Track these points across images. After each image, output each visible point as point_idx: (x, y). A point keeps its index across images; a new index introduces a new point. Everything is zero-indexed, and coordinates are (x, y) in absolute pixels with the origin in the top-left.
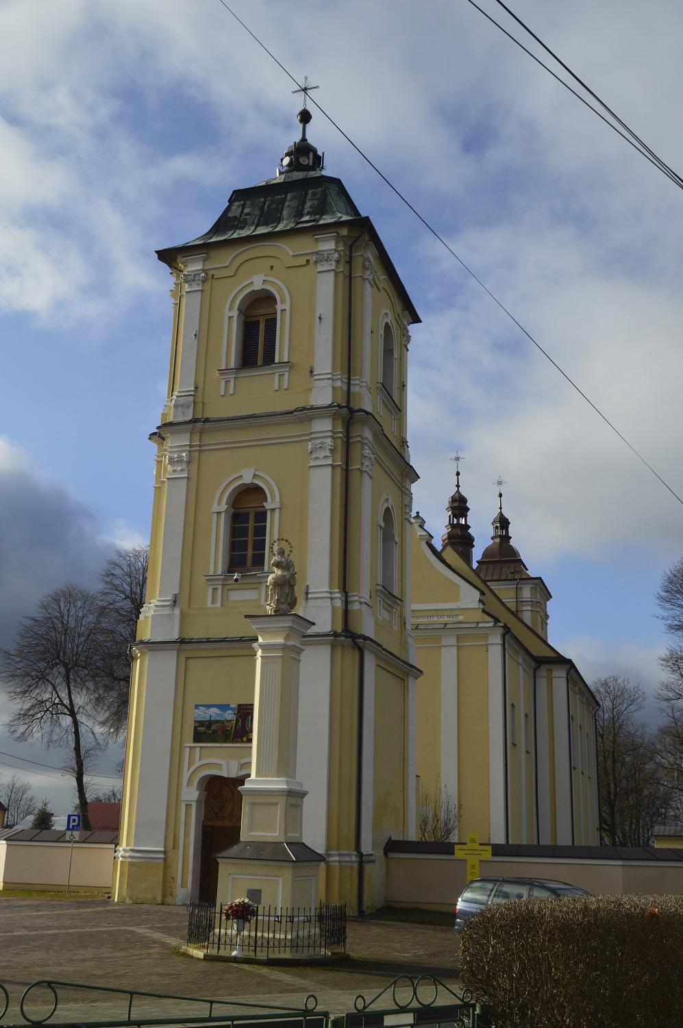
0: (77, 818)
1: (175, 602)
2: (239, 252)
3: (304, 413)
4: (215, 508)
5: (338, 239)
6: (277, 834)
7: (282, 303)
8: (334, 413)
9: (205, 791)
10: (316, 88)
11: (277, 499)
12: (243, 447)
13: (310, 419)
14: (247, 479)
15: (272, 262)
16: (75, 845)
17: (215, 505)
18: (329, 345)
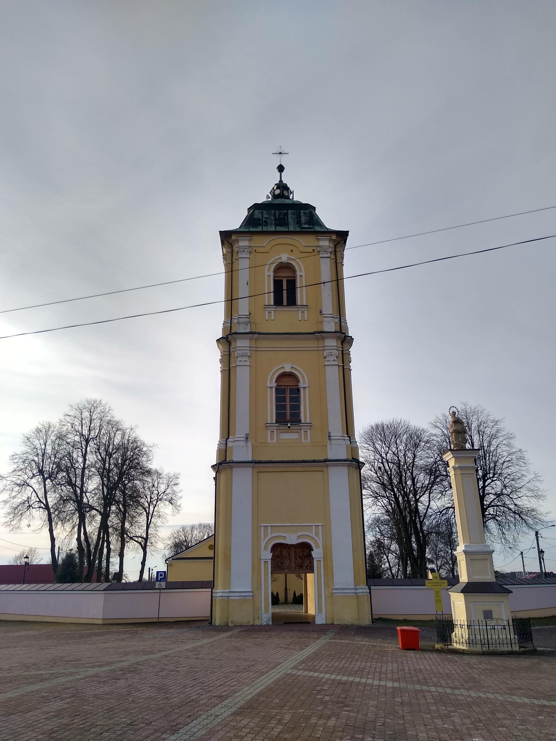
0: (163, 573)
1: (247, 438)
2: (273, 238)
3: (321, 335)
4: (269, 385)
5: (331, 240)
6: (489, 577)
7: (300, 272)
8: (338, 336)
9: (271, 553)
10: (287, 154)
11: (307, 382)
12: (280, 351)
13: (323, 338)
14: (288, 369)
15: (292, 248)
16: (162, 591)
17: (268, 382)
18: (330, 299)
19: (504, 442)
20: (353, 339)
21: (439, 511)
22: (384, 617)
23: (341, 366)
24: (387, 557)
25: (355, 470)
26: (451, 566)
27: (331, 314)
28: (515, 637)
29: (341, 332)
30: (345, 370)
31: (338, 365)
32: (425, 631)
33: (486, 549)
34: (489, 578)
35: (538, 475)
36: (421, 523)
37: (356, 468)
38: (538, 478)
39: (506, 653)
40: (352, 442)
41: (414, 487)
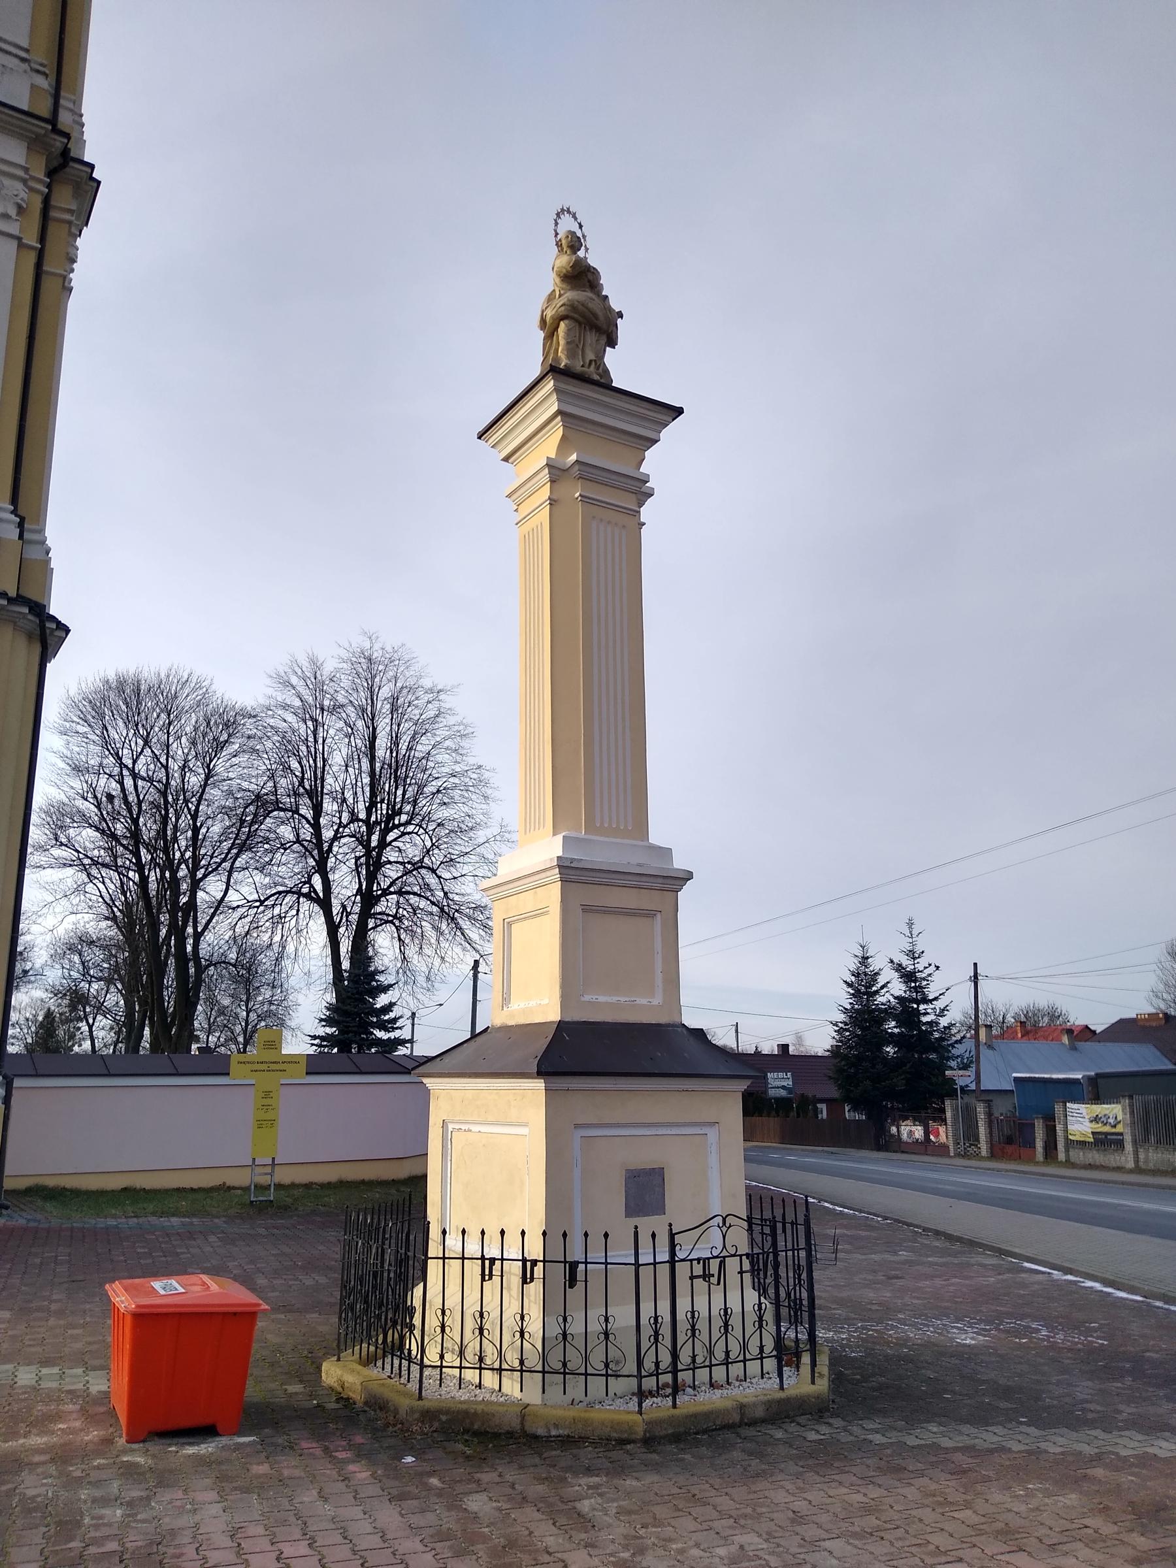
19: (448, 743)
20: (99, 183)
21: (257, 898)
22: (51, 1182)
23: (32, 248)
24: (90, 1027)
25: (21, 643)
26: (241, 1046)
27: (21, 48)
28: (760, 1304)
29: (53, 120)
30: (44, 277)
31: (19, 239)
32: (212, 1238)
33: (654, 866)
34: (655, 1002)
35: (509, 829)
36: (198, 936)
37: (30, 637)
38: (506, 835)
39: (760, 1413)
40: (30, 542)
41: (194, 852)
